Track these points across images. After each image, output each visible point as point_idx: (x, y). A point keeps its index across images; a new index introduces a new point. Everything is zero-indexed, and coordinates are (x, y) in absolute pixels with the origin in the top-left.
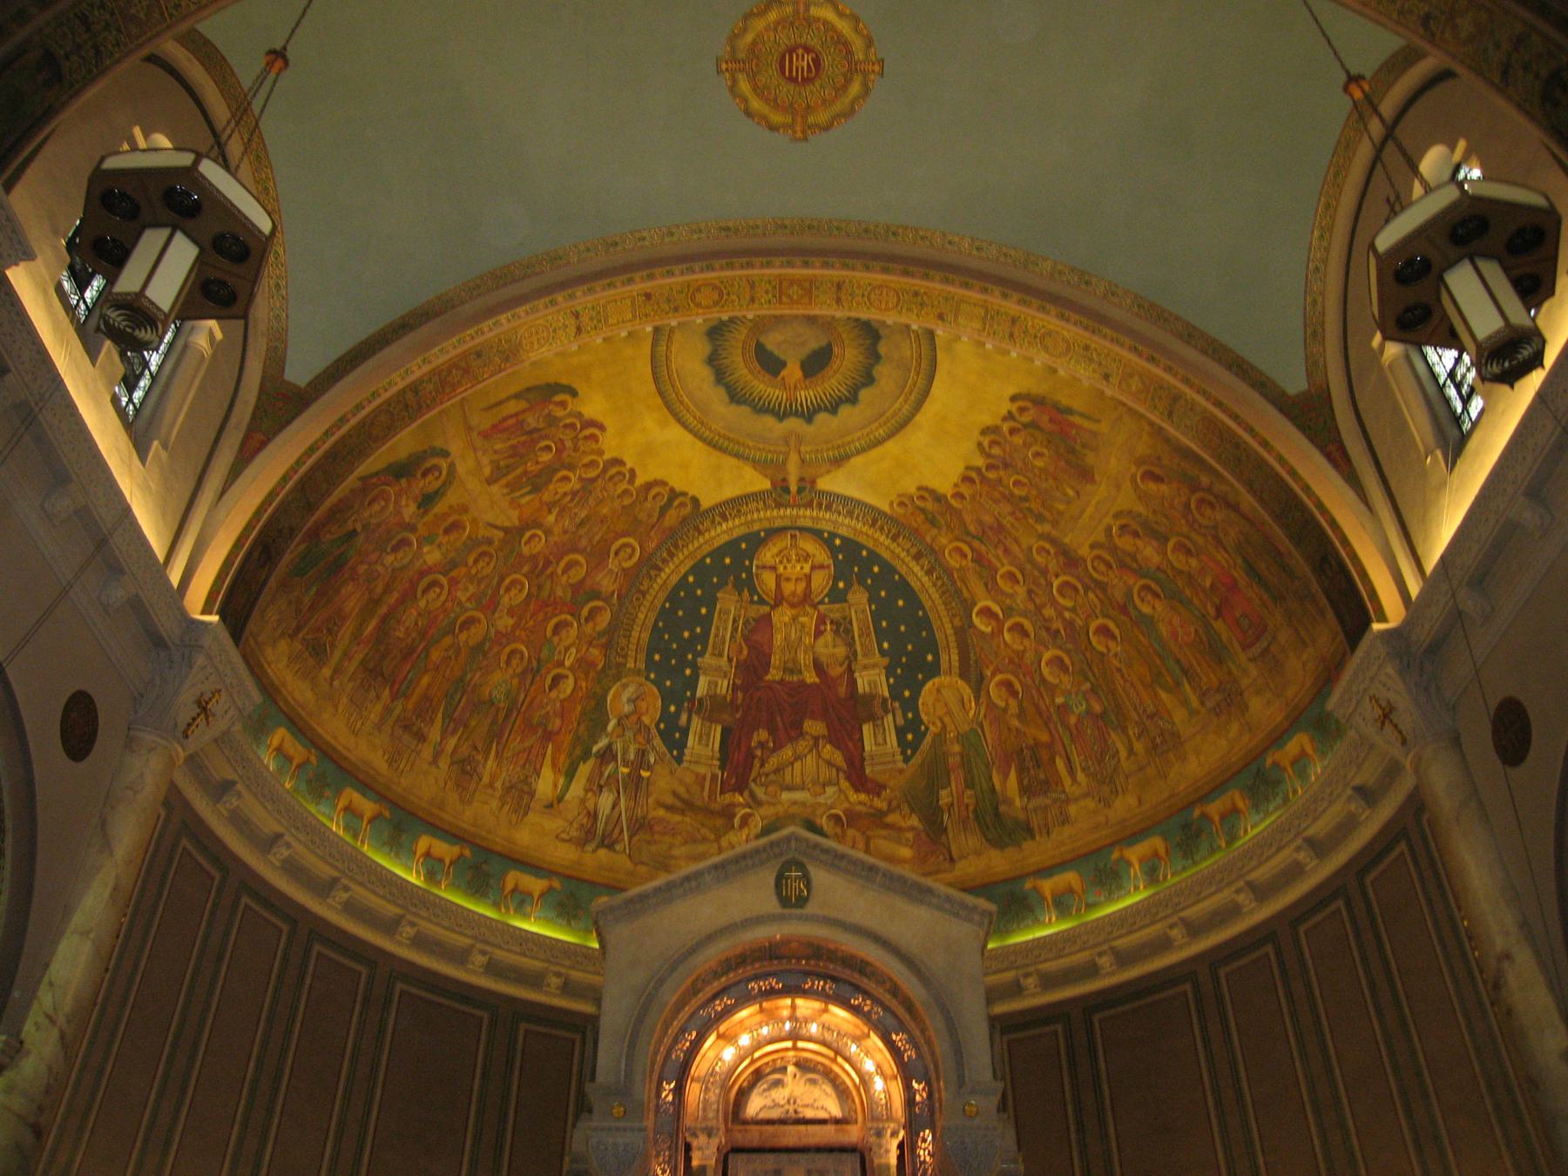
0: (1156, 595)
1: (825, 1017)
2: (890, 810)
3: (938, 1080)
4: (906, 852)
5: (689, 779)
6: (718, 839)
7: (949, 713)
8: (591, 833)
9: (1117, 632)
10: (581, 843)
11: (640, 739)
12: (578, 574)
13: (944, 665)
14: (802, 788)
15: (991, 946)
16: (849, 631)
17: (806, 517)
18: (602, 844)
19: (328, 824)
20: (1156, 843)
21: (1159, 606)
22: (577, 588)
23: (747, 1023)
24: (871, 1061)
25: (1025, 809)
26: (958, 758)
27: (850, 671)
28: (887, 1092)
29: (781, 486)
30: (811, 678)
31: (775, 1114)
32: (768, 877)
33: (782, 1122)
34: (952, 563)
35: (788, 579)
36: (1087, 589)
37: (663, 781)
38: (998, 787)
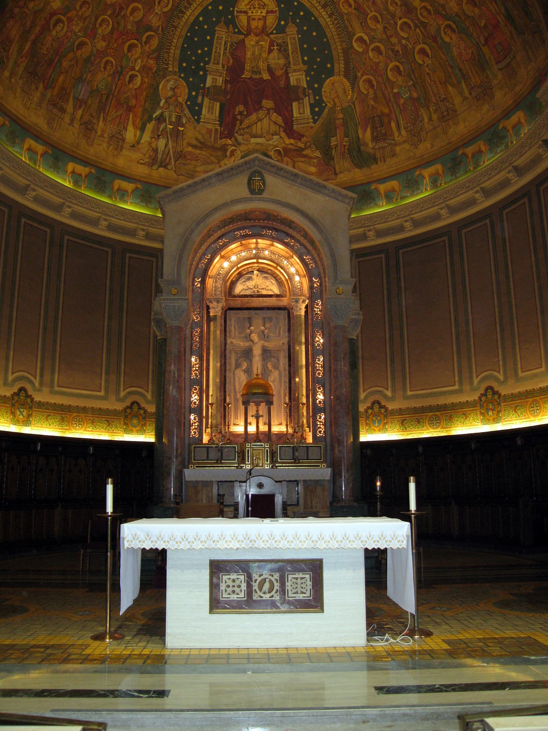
0: (453, 31)
1: (272, 248)
2: (306, 148)
3: (325, 277)
4: (313, 169)
5: (204, 131)
6: (219, 163)
7: (338, 96)
8: (154, 161)
9: (429, 53)
11: (178, 110)
12: (139, 15)
13: (336, 71)
14: (261, 136)
15: (352, 216)
16: (286, 50)
18: (161, 166)
19: (20, 157)
20: (438, 167)
21: (454, 36)
22: (138, 24)
23: (235, 251)
24: (294, 269)
25: (374, 148)
26: (341, 121)
27: (287, 73)
28: (301, 283)
30: (266, 76)
31: (248, 293)
32: (243, 179)
33: (251, 296)
34: (344, 10)
35: (254, 19)
36: (416, 26)
37: (191, 133)
38: (361, 136)
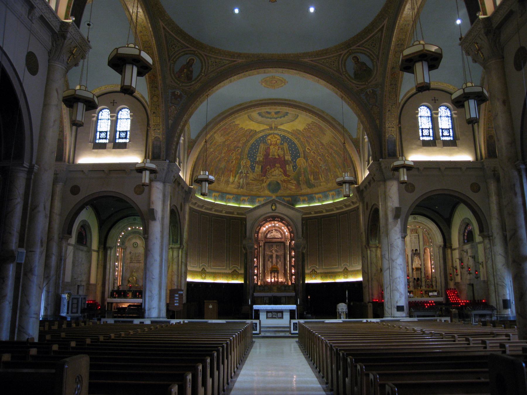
2: (291, 180)
5: (256, 175)
8: (239, 186)
10: (238, 188)
12: (235, 145)
14: (275, 176)
16: (284, 150)
17: (276, 132)
22: (235, 147)
29: (271, 128)
30: (277, 157)
